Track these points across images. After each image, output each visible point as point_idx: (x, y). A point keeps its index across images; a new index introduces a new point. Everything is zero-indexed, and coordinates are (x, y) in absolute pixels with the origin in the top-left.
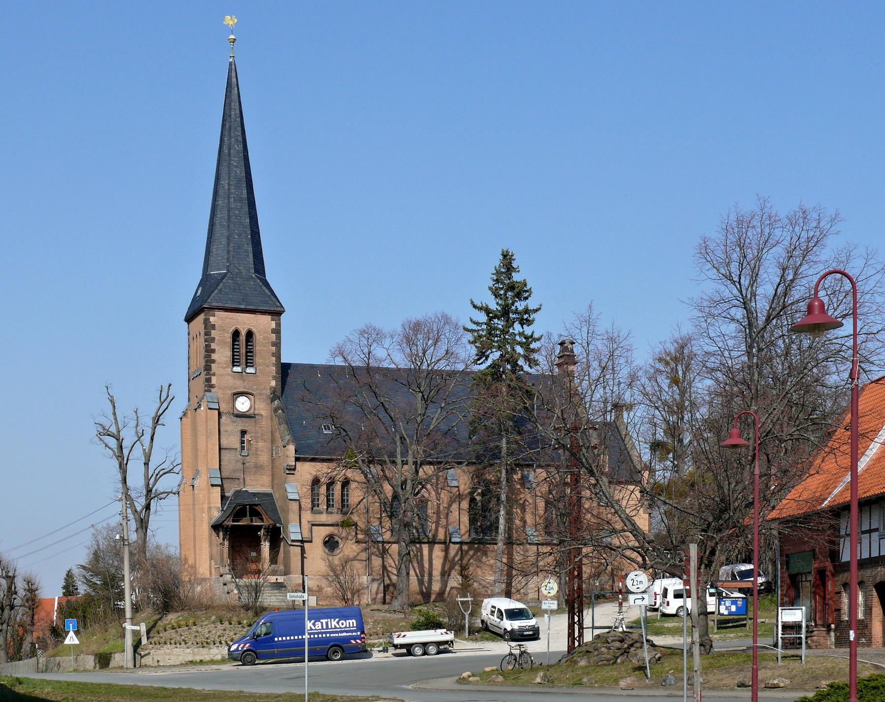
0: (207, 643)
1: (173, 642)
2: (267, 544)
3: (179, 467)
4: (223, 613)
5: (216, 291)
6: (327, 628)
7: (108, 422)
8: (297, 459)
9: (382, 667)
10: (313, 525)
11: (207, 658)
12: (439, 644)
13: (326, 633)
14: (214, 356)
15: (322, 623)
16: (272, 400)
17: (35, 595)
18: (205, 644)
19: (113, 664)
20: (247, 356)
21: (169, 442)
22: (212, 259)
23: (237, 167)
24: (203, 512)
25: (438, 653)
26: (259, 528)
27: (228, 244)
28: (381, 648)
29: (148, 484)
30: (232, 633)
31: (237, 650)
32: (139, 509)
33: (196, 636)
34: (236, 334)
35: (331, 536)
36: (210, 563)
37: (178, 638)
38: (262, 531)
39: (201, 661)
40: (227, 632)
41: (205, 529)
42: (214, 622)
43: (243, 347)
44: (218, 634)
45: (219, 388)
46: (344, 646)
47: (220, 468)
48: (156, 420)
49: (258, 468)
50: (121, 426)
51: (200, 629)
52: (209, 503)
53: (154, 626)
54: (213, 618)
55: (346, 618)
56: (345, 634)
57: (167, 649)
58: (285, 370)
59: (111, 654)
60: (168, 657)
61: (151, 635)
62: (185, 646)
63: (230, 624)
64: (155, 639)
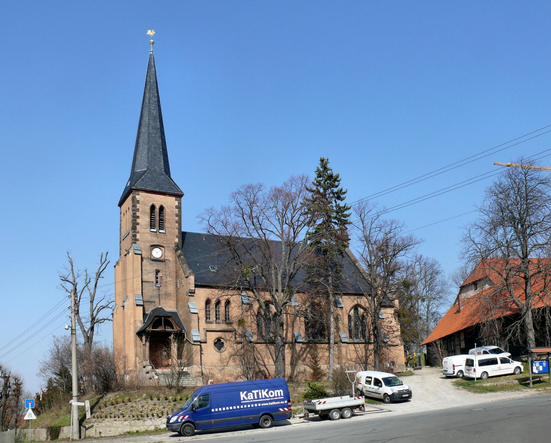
0: (142, 416)
1: (112, 415)
2: (176, 344)
3: (114, 303)
4: (154, 392)
5: (140, 180)
6: (258, 398)
7: (66, 273)
8: (196, 286)
9: (298, 433)
10: (207, 331)
11: (142, 429)
12: (352, 408)
13: (257, 403)
14: (138, 221)
15: (253, 394)
16: (176, 251)
17: (20, 388)
18: (140, 417)
19: (61, 436)
20: (160, 223)
21: (107, 290)
22: (137, 163)
23: (154, 110)
24: (130, 324)
25: (353, 415)
26: (170, 334)
27: (148, 154)
28: (302, 415)
29: (93, 314)
30: (161, 407)
31: (177, 421)
32: (86, 330)
33: (132, 411)
34: (153, 207)
35: (219, 340)
36: (136, 360)
37: (117, 412)
38: (172, 336)
39: (137, 432)
40: (157, 406)
41: (131, 335)
42: (145, 399)
43: (157, 217)
44: (150, 408)
45: (142, 241)
46: (273, 414)
47: (142, 295)
48: (99, 275)
49: (167, 295)
50: (76, 276)
51: (134, 405)
52: (135, 317)
53: (97, 403)
54: (144, 395)
55: (274, 388)
56: (274, 403)
57: (107, 422)
58: (183, 235)
59: (60, 427)
60: (108, 429)
61: (94, 410)
62: (123, 419)
63: (159, 400)
64: (98, 413)
